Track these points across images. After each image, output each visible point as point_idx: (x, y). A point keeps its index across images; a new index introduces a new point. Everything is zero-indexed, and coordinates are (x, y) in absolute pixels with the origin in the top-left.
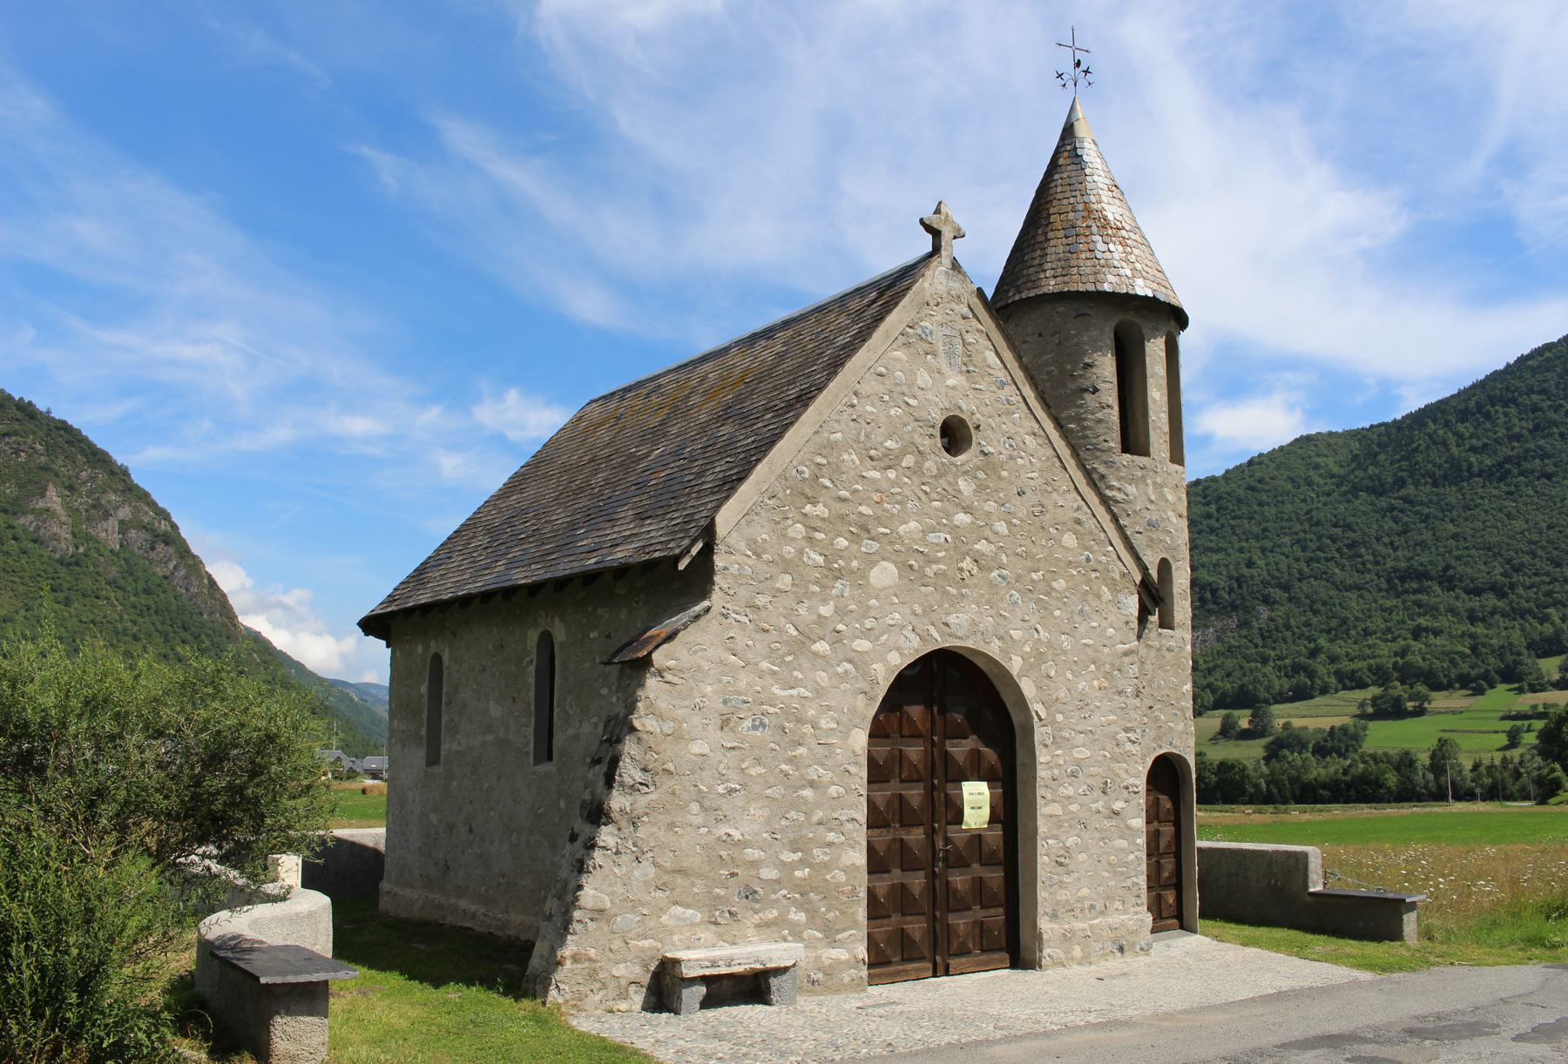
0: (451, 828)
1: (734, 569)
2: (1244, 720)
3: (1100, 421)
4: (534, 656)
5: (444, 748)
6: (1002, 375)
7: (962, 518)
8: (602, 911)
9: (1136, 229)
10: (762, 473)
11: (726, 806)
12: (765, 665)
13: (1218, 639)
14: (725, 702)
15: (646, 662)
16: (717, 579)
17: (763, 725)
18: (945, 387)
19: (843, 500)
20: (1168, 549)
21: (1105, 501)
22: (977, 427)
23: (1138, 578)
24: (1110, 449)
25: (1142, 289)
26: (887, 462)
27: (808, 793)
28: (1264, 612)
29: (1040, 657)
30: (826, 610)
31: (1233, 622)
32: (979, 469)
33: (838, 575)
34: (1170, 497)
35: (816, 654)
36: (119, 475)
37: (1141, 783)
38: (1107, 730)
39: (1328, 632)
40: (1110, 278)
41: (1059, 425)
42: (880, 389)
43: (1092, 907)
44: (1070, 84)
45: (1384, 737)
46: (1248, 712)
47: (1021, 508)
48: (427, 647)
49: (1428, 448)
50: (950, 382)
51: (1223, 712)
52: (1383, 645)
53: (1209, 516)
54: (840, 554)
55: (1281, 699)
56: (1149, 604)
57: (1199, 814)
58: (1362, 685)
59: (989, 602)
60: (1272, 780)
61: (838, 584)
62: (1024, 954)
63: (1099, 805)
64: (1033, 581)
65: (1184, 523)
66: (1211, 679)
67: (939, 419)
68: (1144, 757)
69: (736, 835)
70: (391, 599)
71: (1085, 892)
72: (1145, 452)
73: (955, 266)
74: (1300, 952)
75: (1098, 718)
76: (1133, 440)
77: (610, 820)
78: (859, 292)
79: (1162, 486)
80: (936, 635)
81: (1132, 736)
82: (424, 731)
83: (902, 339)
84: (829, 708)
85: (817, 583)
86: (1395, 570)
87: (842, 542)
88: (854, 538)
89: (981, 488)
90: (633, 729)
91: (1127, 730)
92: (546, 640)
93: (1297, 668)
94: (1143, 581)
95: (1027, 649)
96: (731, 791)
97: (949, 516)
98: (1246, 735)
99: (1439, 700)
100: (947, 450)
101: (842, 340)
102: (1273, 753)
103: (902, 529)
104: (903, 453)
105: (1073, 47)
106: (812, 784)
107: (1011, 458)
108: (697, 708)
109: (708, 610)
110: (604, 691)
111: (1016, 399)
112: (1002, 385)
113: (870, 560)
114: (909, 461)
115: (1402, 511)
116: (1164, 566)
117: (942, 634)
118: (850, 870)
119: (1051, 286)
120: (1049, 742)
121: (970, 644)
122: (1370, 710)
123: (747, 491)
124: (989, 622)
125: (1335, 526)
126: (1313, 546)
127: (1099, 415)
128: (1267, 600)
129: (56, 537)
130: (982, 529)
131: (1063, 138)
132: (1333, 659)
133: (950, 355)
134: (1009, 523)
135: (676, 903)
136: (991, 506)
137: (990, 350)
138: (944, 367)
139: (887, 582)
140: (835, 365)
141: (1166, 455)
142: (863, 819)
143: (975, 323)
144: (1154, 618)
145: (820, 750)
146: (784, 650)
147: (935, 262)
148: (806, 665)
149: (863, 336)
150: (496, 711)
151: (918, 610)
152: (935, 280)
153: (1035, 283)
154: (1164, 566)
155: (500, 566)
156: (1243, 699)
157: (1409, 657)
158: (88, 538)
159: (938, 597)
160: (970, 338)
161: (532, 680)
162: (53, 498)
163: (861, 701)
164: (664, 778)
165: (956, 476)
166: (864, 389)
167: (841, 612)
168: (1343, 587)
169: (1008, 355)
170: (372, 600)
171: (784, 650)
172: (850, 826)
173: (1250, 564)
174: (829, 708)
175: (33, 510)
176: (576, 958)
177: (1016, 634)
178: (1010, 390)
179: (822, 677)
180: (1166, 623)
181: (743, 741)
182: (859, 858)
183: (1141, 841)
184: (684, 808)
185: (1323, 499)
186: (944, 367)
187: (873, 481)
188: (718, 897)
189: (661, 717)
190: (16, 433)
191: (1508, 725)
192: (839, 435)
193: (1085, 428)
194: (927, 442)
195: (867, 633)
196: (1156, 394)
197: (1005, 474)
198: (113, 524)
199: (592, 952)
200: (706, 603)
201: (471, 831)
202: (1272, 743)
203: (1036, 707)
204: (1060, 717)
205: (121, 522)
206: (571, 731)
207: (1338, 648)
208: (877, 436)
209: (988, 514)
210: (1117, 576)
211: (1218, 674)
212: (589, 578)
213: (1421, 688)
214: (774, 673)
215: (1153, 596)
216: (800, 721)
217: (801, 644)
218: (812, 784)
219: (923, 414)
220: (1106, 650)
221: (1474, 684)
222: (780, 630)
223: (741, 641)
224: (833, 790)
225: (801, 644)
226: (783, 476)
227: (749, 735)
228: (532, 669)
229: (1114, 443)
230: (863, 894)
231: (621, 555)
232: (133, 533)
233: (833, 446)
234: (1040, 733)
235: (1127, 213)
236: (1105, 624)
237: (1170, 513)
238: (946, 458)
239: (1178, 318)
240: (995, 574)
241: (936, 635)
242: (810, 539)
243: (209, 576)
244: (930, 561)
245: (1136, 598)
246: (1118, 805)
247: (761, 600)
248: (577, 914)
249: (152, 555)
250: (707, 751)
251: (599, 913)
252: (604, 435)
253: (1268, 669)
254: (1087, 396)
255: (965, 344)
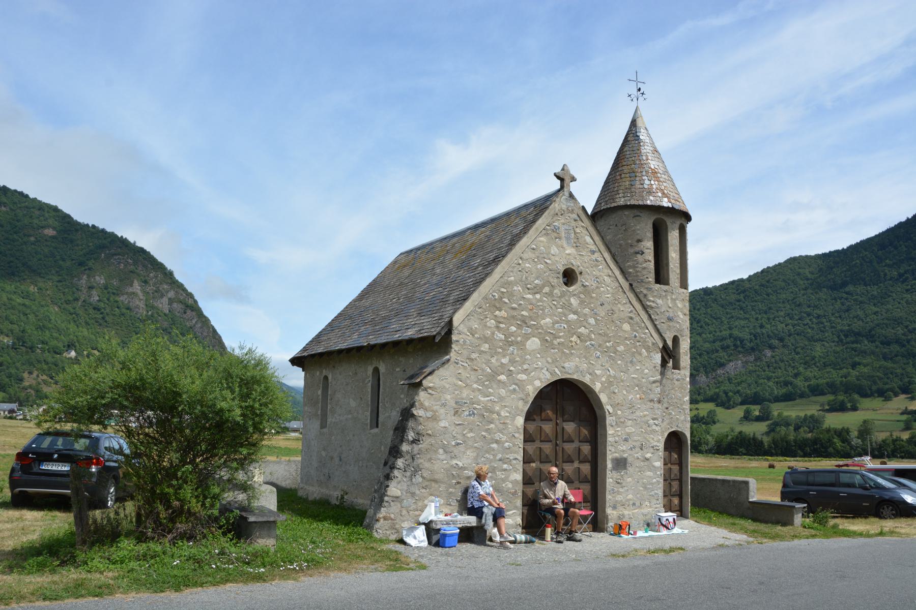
0: (332, 458)
1: (461, 341)
2: (756, 411)
3: (644, 268)
4: (370, 379)
5: (329, 420)
6: (593, 248)
7: (572, 317)
8: (397, 497)
9: (666, 172)
10: (476, 297)
11: (456, 451)
12: (475, 386)
13: (743, 367)
14: (456, 403)
15: (420, 384)
16: (453, 346)
17: (474, 414)
18: (565, 254)
19: (514, 309)
20: (678, 330)
21: (645, 308)
22: (581, 273)
23: (661, 346)
24: (649, 282)
25: (665, 203)
26: (536, 290)
27: (494, 446)
28: (769, 353)
29: (610, 384)
30: (505, 361)
31: (752, 358)
32: (581, 293)
33: (511, 344)
34: (679, 305)
35: (500, 381)
36: (169, 275)
37: (661, 446)
38: (643, 419)
39: (805, 364)
40: (651, 198)
41: (623, 272)
42: (533, 256)
43: (634, 504)
44: (635, 99)
45: (834, 421)
46: (758, 407)
47: (602, 312)
48: (321, 372)
49: (861, 264)
50: (567, 252)
51: (745, 407)
52: (834, 372)
53: (739, 301)
54: (512, 334)
55: (777, 400)
56: (666, 358)
57: (691, 458)
58: (822, 393)
59: (585, 357)
60: (774, 442)
61: (511, 349)
62: (599, 525)
63: (639, 455)
64: (607, 347)
65: (687, 318)
66: (740, 388)
67: (562, 269)
68: (663, 432)
69: (461, 464)
70: (305, 349)
71: (630, 496)
72: (667, 283)
73: (571, 196)
74: (710, 523)
75: (639, 413)
76: (661, 277)
77: (401, 456)
78: (526, 206)
79: (675, 300)
80: (558, 372)
81: (656, 422)
82: (319, 412)
83: (544, 232)
84: (505, 406)
85: (501, 347)
86: (842, 331)
87: (513, 329)
88: (519, 327)
89: (582, 302)
90: (413, 416)
91: (654, 419)
92: (376, 370)
93: (786, 384)
94: (664, 347)
95: (604, 379)
96: (458, 444)
97: (566, 316)
98: (758, 419)
99: (866, 403)
100: (566, 284)
101: (516, 231)
102: (771, 430)
103: (542, 322)
104: (543, 286)
105: (637, 81)
106: (497, 442)
107: (597, 287)
108: (444, 405)
109: (448, 360)
110: (402, 396)
111: (600, 259)
112: (593, 252)
113: (527, 337)
114: (547, 289)
115: (846, 299)
116: (676, 340)
117: (561, 372)
118: (515, 482)
119: (621, 202)
120: (614, 424)
121: (575, 377)
122: (827, 407)
123: (468, 306)
124: (585, 366)
125: (809, 307)
126: (797, 318)
127: (644, 265)
128: (771, 347)
129: (137, 307)
130: (582, 322)
131: (630, 127)
132: (806, 379)
133: (568, 239)
134: (596, 319)
135: (431, 495)
136: (587, 311)
137: (589, 238)
138: (565, 245)
139: (534, 347)
140: (512, 244)
141: (678, 284)
142: (521, 459)
143: (580, 223)
144: (670, 364)
145: (501, 426)
146: (485, 379)
147: (561, 194)
148: (495, 386)
149: (525, 231)
150: (353, 404)
151: (549, 360)
152: (560, 204)
153: (614, 200)
154: (676, 340)
155: (355, 336)
156: (756, 399)
157: (849, 378)
158: (153, 307)
159: (560, 354)
160: (578, 230)
161: (369, 390)
162: (137, 287)
163: (521, 403)
164: (427, 437)
165: (570, 297)
166: (525, 256)
167: (512, 362)
168: (811, 339)
169: (597, 238)
170: (294, 351)
171: (485, 379)
172: (515, 462)
173: (762, 326)
174: (505, 406)
175: (127, 293)
176: (385, 518)
177: (598, 372)
178: (597, 255)
179: (503, 392)
180: (676, 366)
181: (464, 421)
182: (519, 477)
183: (660, 472)
184: (436, 452)
185: (802, 292)
186: (565, 245)
187: (529, 299)
188: (451, 493)
189: (426, 409)
190: (119, 254)
191: (904, 417)
192: (512, 278)
193: (638, 272)
194: (556, 281)
195: (525, 371)
196: (673, 255)
197: (594, 295)
198: (165, 300)
199: (392, 516)
200: (448, 357)
201: (340, 460)
202: (772, 424)
203: (608, 408)
204: (619, 412)
205: (170, 299)
206: (387, 414)
207: (808, 373)
208: (531, 279)
209: (586, 315)
210: (650, 344)
211: (744, 385)
212: (396, 344)
213: (856, 396)
214: (479, 390)
215: (669, 354)
216: (492, 412)
217: (492, 377)
218: (497, 442)
219: (554, 267)
220: (644, 380)
221: (884, 394)
222: (483, 370)
223: (465, 374)
224: (507, 444)
225: (492, 377)
226: (485, 298)
227: (472, 416)
228: (370, 384)
229: (652, 278)
230: (520, 494)
231: (410, 333)
232: (175, 305)
233: (509, 284)
234: (609, 420)
235: (661, 165)
236: (643, 368)
237: (679, 313)
238: (565, 288)
239: (687, 217)
240: (588, 343)
241: (558, 372)
242: (497, 327)
243: (213, 327)
244: (556, 337)
245: (660, 355)
246: (648, 455)
247: (474, 356)
248: (386, 498)
249: (185, 316)
250: (447, 425)
251: (396, 498)
252: (406, 272)
253: (771, 384)
254: (639, 256)
255: (575, 233)
